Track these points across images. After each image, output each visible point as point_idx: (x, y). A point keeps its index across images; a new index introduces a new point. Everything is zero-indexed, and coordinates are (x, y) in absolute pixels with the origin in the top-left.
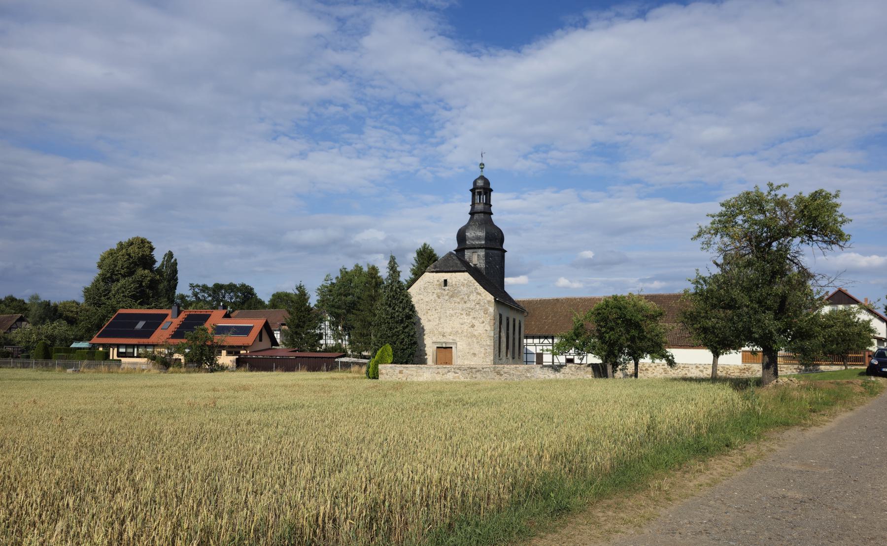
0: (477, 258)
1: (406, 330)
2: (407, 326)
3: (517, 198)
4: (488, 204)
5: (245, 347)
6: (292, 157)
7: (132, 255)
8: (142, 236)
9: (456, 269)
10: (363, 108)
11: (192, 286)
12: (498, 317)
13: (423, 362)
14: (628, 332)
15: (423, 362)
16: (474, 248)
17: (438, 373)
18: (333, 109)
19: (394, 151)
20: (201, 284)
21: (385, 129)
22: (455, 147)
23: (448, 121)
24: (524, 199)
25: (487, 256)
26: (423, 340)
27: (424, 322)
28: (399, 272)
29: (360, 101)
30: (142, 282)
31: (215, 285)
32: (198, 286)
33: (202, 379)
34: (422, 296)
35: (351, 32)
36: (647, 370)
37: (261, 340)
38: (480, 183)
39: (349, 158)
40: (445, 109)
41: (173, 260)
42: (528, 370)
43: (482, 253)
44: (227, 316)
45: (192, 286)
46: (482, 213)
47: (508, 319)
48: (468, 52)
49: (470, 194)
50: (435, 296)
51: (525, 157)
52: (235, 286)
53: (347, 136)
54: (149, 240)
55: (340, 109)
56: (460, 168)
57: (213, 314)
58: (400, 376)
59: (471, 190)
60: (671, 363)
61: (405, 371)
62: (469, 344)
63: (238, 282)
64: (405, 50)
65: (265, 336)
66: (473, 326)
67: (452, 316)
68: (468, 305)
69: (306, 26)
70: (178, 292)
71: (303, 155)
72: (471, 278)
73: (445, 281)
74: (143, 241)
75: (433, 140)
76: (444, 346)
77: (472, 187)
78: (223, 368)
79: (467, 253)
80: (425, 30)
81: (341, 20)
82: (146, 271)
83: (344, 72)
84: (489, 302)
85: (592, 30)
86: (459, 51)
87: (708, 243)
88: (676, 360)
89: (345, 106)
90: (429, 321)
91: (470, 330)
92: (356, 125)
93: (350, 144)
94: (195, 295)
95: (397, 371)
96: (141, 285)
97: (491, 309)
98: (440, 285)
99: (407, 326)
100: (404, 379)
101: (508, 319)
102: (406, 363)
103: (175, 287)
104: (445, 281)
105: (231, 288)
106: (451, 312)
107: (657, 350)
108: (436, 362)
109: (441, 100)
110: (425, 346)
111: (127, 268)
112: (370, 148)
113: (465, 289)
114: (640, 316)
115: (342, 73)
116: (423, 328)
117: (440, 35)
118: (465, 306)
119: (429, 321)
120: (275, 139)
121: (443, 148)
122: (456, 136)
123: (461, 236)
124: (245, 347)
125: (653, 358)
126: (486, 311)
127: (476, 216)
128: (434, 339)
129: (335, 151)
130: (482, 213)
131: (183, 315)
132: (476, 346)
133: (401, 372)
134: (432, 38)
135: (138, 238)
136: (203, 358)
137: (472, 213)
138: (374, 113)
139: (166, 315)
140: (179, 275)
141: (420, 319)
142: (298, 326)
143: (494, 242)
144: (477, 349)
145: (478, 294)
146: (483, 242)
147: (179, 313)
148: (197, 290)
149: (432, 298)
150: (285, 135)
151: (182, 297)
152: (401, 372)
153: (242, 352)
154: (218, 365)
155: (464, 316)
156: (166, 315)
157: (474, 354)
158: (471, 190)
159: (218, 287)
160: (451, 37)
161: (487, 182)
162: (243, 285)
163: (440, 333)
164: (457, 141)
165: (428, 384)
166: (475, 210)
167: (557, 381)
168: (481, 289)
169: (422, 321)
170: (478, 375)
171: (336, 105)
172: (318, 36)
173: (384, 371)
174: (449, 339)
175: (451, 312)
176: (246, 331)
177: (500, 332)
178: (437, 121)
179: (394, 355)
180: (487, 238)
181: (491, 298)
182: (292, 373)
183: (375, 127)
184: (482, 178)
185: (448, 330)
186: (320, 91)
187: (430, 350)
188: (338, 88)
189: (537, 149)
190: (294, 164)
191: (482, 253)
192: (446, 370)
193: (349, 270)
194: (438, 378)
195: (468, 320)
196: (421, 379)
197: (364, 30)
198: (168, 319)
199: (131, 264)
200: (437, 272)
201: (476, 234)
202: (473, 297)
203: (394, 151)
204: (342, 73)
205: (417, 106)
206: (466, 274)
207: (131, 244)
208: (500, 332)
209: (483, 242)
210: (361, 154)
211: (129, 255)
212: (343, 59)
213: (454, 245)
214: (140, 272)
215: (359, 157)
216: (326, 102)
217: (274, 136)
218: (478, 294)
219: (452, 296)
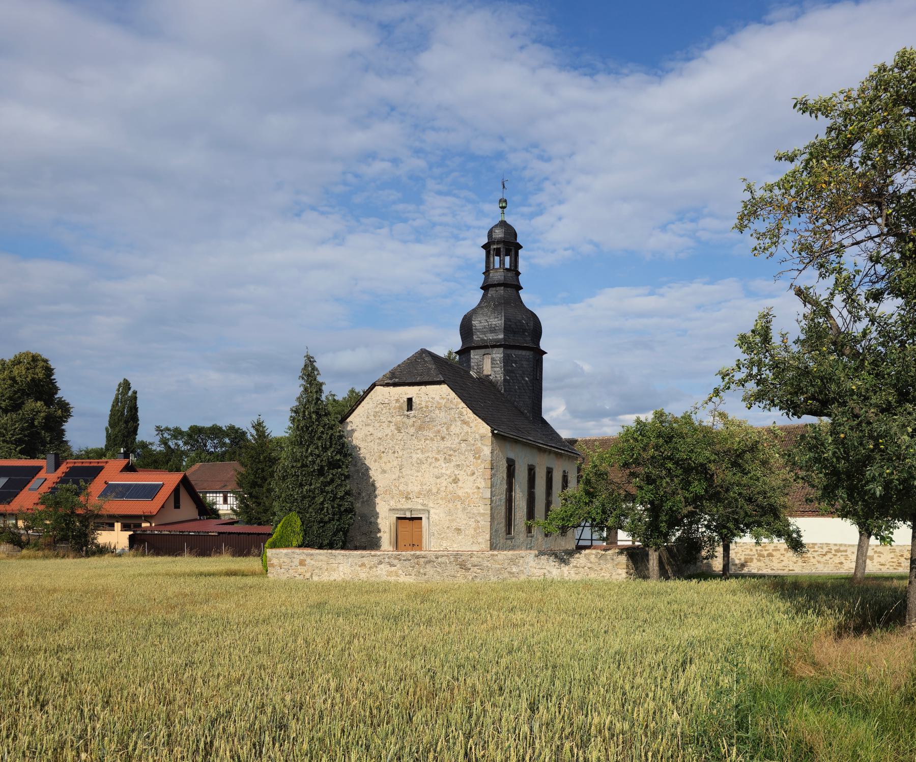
0: (489, 365)
1: (328, 488)
2: (332, 481)
3: (651, 294)
4: (514, 270)
5: (147, 518)
6: (323, 242)
7: (18, 379)
8: (34, 350)
9: (426, 379)
10: (420, 163)
11: (159, 429)
12: (504, 465)
13: (372, 544)
14: (686, 484)
15: (372, 544)
16: (485, 346)
17: (363, 565)
18: (378, 167)
19: (468, 228)
20: (171, 426)
21: (455, 195)
22: (560, 219)
23: (547, 179)
24: (662, 295)
25: (507, 361)
26: (374, 505)
27: (375, 474)
28: (321, 384)
29: (418, 152)
30: (33, 419)
31: (191, 428)
32: (168, 429)
33: (67, 572)
34: (371, 429)
35: (402, 41)
36: (770, 555)
37: (177, 506)
38: (499, 234)
39: (405, 242)
40: (541, 158)
41: (130, 393)
42: (513, 561)
43: (498, 354)
44: (129, 468)
45: (159, 429)
46: (503, 288)
47: (531, 470)
48: (575, 68)
49: (484, 252)
50: (393, 428)
51: (664, 228)
52: (220, 429)
53: (401, 207)
54: (45, 356)
55: (386, 165)
56: (566, 249)
57: (107, 466)
58: (301, 569)
59: (484, 247)
60: (796, 545)
61: (308, 561)
62: (449, 513)
63: (223, 424)
64: (489, 76)
65: (185, 498)
66: (456, 481)
67: (422, 463)
68: (448, 443)
69: (338, 39)
70: (139, 438)
71: (338, 239)
72: (453, 395)
73: (410, 401)
74: (35, 359)
75: (525, 210)
76: (408, 515)
77: (485, 241)
78: (102, 551)
79: (475, 356)
80: (512, 36)
81: (386, 28)
82: (39, 404)
83: (393, 109)
84: (482, 437)
85: (770, 23)
86: (562, 67)
87: (774, 235)
88: (804, 540)
89: (395, 161)
90: (384, 472)
91: (451, 487)
92: (411, 190)
93: (405, 221)
94: (164, 442)
95: (296, 562)
96: (32, 425)
97: (487, 451)
98: (401, 408)
99: (332, 481)
100: (308, 575)
101: (531, 470)
102: (331, 546)
103: (135, 431)
104: (410, 401)
105: (215, 432)
106: (420, 456)
107: (769, 518)
108: (397, 545)
109: (535, 146)
110: (376, 515)
111: (10, 398)
112: (434, 225)
113: (443, 414)
114: (707, 454)
115: (390, 109)
116: (373, 485)
117: (535, 41)
118: (442, 445)
119: (384, 472)
120: (298, 215)
121: (539, 221)
122: (561, 202)
123: (466, 329)
124: (147, 518)
125: (757, 537)
126: (477, 455)
127: (492, 292)
128: (393, 503)
129: (385, 231)
130: (503, 288)
131: (63, 468)
132: (460, 514)
133: (302, 563)
134: (522, 48)
135: (27, 354)
136: (72, 535)
137: (485, 288)
138: (437, 171)
139: (39, 469)
140: (142, 414)
141: (368, 469)
142: (254, 484)
143: (524, 338)
144: (462, 520)
145: (465, 422)
146: (501, 336)
147: (57, 466)
148: (166, 435)
149: (388, 431)
150: (313, 208)
151: (144, 445)
152: (302, 563)
153: (144, 525)
154: (98, 546)
155: (441, 462)
156: (39, 469)
157: (458, 530)
158: (484, 247)
159: (196, 433)
160: (551, 45)
161: (510, 232)
162: (232, 428)
163: (401, 493)
164: (562, 209)
165: (342, 587)
166: (490, 282)
167: (563, 582)
168: (469, 414)
169: (371, 473)
170: (429, 569)
171: (383, 160)
172: (353, 54)
173: (275, 561)
174: (415, 505)
175: (420, 456)
176: (150, 492)
177: (510, 489)
178: (531, 180)
179: (306, 533)
180: (507, 329)
181: (485, 429)
182: (206, 559)
183: (440, 193)
184: (503, 224)
185: (414, 488)
186: (359, 139)
187: (385, 522)
188: (385, 134)
189: (681, 216)
190: (327, 253)
191: (498, 354)
192: (375, 560)
193: (339, 398)
194: (363, 575)
195: (447, 469)
196: (326, 578)
197: (421, 41)
198: (42, 474)
199: (15, 392)
200: (395, 385)
201: (491, 324)
202: (456, 429)
203: (468, 228)
204: (390, 109)
205: (500, 156)
206: (444, 389)
207: (17, 362)
208: (510, 489)
209: (501, 336)
210: (421, 235)
211: (13, 379)
212: (390, 88)
213: (456, 343)
214: (33, 405)
215: (418, 241)
216: (369, 156)
217: (296, 212)
218: (465, 422)
219: (420, 428)
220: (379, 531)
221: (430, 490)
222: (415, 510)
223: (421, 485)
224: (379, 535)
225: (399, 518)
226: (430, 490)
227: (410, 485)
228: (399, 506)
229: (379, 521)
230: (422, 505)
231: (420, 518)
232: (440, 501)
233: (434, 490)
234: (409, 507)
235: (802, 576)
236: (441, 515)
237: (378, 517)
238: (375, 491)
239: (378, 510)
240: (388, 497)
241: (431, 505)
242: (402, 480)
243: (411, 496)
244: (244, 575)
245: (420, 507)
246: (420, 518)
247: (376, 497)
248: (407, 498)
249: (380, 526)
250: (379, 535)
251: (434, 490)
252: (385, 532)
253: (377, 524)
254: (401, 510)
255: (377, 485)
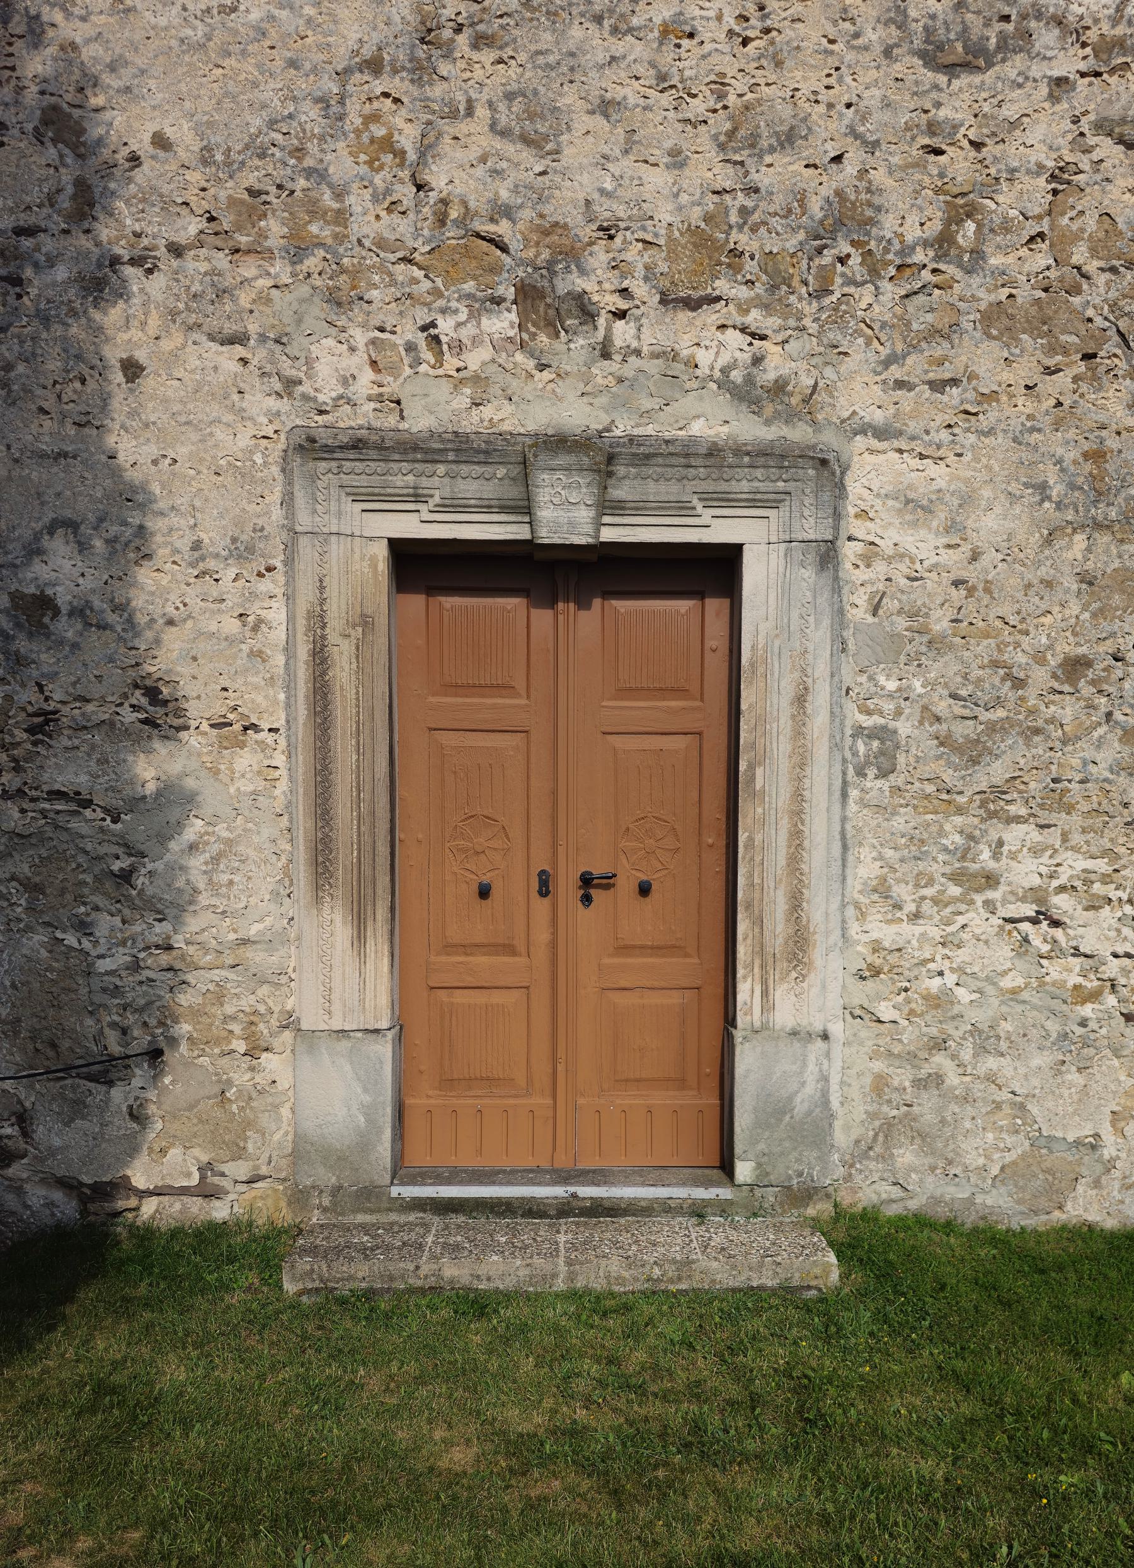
26: (81, 396)
76: (565, 514)
110: (118, 525)
128: (338, 370)
163: (467, 246)
220: (159, 710)
221: (850, 217)
222: (645, 455)
223: (740, 140)
224: (148, 769)
225: (417, 566)
226: (850, 217)
227: (584, 141)
228: (433, 406)
229: (156, 587)
230: (747, 393)
231: (714, 571)
232: (982, 358)
233: (908, 220)
234: (575, 414)
235: (201, 929)
236: (990, 524)
237: (135, 547)
238: (86, 204)
239: (131, 450)
240: (263, 285)
241: (859, 394)
242: (472, 73)
243: (594, 281)
244: (798, 733)
245: (709, 421)
246: (714, 571)
247: (100, 282)
248: (549, 307)
249: (171, 658)
250: (148, 769)
251: (908, 220)
252: (233, 729)
253: (110, 619)
254: (462, 449)
255: (125, 125)
